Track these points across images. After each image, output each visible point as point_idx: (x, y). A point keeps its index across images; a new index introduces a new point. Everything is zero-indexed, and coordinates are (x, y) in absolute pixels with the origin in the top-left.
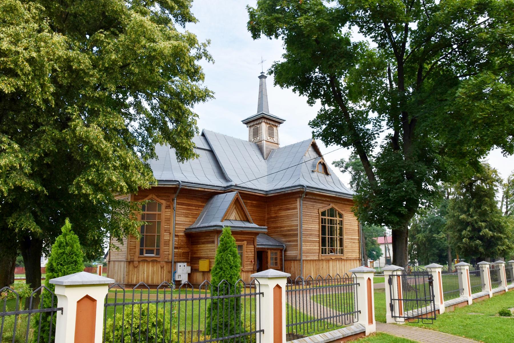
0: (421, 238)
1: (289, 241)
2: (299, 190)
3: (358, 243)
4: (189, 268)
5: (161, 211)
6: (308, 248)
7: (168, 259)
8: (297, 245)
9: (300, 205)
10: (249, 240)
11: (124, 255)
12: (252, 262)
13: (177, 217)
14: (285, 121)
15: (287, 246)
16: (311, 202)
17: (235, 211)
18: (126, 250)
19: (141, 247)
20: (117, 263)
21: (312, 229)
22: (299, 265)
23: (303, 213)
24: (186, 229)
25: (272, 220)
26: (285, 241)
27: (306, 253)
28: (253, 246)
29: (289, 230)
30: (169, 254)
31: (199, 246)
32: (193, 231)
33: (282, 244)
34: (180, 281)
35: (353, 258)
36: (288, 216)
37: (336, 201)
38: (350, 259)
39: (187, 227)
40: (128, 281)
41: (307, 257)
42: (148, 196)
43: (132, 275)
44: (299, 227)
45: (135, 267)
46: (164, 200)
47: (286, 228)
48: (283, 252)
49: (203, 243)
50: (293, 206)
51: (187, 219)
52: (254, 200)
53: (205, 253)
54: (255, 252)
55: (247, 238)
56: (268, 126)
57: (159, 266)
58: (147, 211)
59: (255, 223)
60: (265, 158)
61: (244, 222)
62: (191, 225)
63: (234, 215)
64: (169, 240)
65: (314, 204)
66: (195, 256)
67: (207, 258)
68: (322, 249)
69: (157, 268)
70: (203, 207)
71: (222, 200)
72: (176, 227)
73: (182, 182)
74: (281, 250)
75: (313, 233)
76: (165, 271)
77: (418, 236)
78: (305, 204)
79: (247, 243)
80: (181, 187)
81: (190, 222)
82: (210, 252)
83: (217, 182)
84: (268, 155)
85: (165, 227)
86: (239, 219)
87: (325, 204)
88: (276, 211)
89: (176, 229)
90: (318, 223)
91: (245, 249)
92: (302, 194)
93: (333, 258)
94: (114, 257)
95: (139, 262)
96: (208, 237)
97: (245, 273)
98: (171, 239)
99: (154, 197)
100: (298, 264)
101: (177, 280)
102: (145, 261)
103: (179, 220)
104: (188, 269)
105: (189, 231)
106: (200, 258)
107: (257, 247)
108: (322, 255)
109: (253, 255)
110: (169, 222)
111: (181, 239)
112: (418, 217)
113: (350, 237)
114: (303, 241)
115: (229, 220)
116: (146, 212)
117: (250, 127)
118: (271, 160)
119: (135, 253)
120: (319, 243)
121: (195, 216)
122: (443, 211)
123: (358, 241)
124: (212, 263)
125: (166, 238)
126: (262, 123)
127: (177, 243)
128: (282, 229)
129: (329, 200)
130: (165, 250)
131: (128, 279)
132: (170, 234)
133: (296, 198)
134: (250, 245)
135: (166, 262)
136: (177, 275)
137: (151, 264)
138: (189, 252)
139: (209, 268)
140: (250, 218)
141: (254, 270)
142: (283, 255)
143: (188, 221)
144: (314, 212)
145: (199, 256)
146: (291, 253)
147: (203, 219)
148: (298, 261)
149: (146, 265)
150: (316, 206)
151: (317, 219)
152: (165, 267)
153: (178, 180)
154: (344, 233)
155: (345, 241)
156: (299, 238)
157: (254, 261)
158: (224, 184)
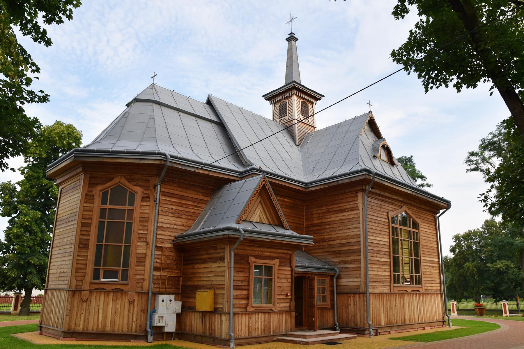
0: (471, 268)
1: (345, 262)
2: (363, 177)
3: (438, 269)
4: (180, 304)
6: (375, 273)
7: (142, 287)
8: (360, 267)
10: (283, 258)
12: (287, 295)
13: (160, 216)
14: (323, 96)
15: (342, 270)
16: (378, 200)
17: (260, 206)
18: (70, 270)
19: (95, 265)
20: (56, 293)
21: (380, 243)
22: (364, 301)
23: (368, 216)
24: (176, 237)
25: (315, 228)
26: (337, 262)
27: (373, 282)
28: (289, 269)
29: (344, 245)
30: (144, 280)
31: (196, 266)
32: (188, 240)
33: (333, 267)
34: (162, 327)
35: (433, 291)
36: (341, 222)
38: (430, 292)
39: (176, 234)
40: (69, 326)
41: (374, 289)
42: (113, 178)
43: (77, 314)
44: (362, 239)
45: (83, 301)
46: (140, 186)
47: (338, 242)
48: (335, 280)
49: (204, 261)
50: (351, 205)
51: (179, 221)
52: (288, 197)
53: (208, 279)
54: (292, 278)
55: (280, 255)
56: (300, 101)
57: (126, 300)
58: (110, 204)
59: (292, 229)
60: (297, 144)
61: (275, 227)
62: (186, 231)
63: (258, 214)
64: (146, 255)
65: (382, 203)
66: (189, 283)
67: (210, 288)
68: (394, 275)
69: (122, 304)
70: (206, 202)
71: (238, 190)
72: (159, 232)
73: (171, 156)
74: (332, 277)
76: (135, 310)
77: (466, 266)
78: (369, 203)
80: (168, 164)
81: (183, 225)
82: (216, 276)
83: (228, 164)
84: (301, 140)
85: (140, 232)
86: (267, 222)
87: (396, 205)
88: (321, 215)
89: (158, 237)
90: (387, 234)
91: (277, 272)
92: (366, 185)
93: (409, 290)
94: (54, 283)
95: (91, 292)
97: (276, 316)
98: (149, 253)
99: (123, 181)
100: (362, 300)
101: (156, 325)
102: (101, 290)
103: (163, 220)
104: (178, 306)
105: (180, 241)
106: (198, 287)
107: (296, 269)
108: (395, 285)
109: (289, 284)
110: (146, 224)
111: (167, 253)
112: (464, 242)
113: (429, 259)
114: (369, 262)
115: (250, 222)
116: (108, 206)
117: (275, 103)
118: (305, 146)
120: (390, 265)
121: (193, 217)
122: (514, 231)
123: (437, 265)
124: (219, 297)
125: (140, 252)
126: (293, 97)
127: (158, 261)
128: (332, 243)
129: (402, 200)
130: (138, 272)
131: (70, 321)
132: (148, 244)
133: (356, 192)
134: (284, 266)
135: (139, 293)
136: (156, 317)
137: (111, 295)
138: (180, 277)
139: (213, 306)
140: (284, 220)
141: (290, 309)
142: (335, 285)
143: (180, 223)
144: (382, 216)
145: (196, 283)
146: (347, 282)
147: (205, 221)
148: (361, 295)
150: (384, 207)
153: (165, 152)
154: (421, 252)
155: (422, 264)
156: (362, 257)
157: (291, 295)
158: (241, 169)
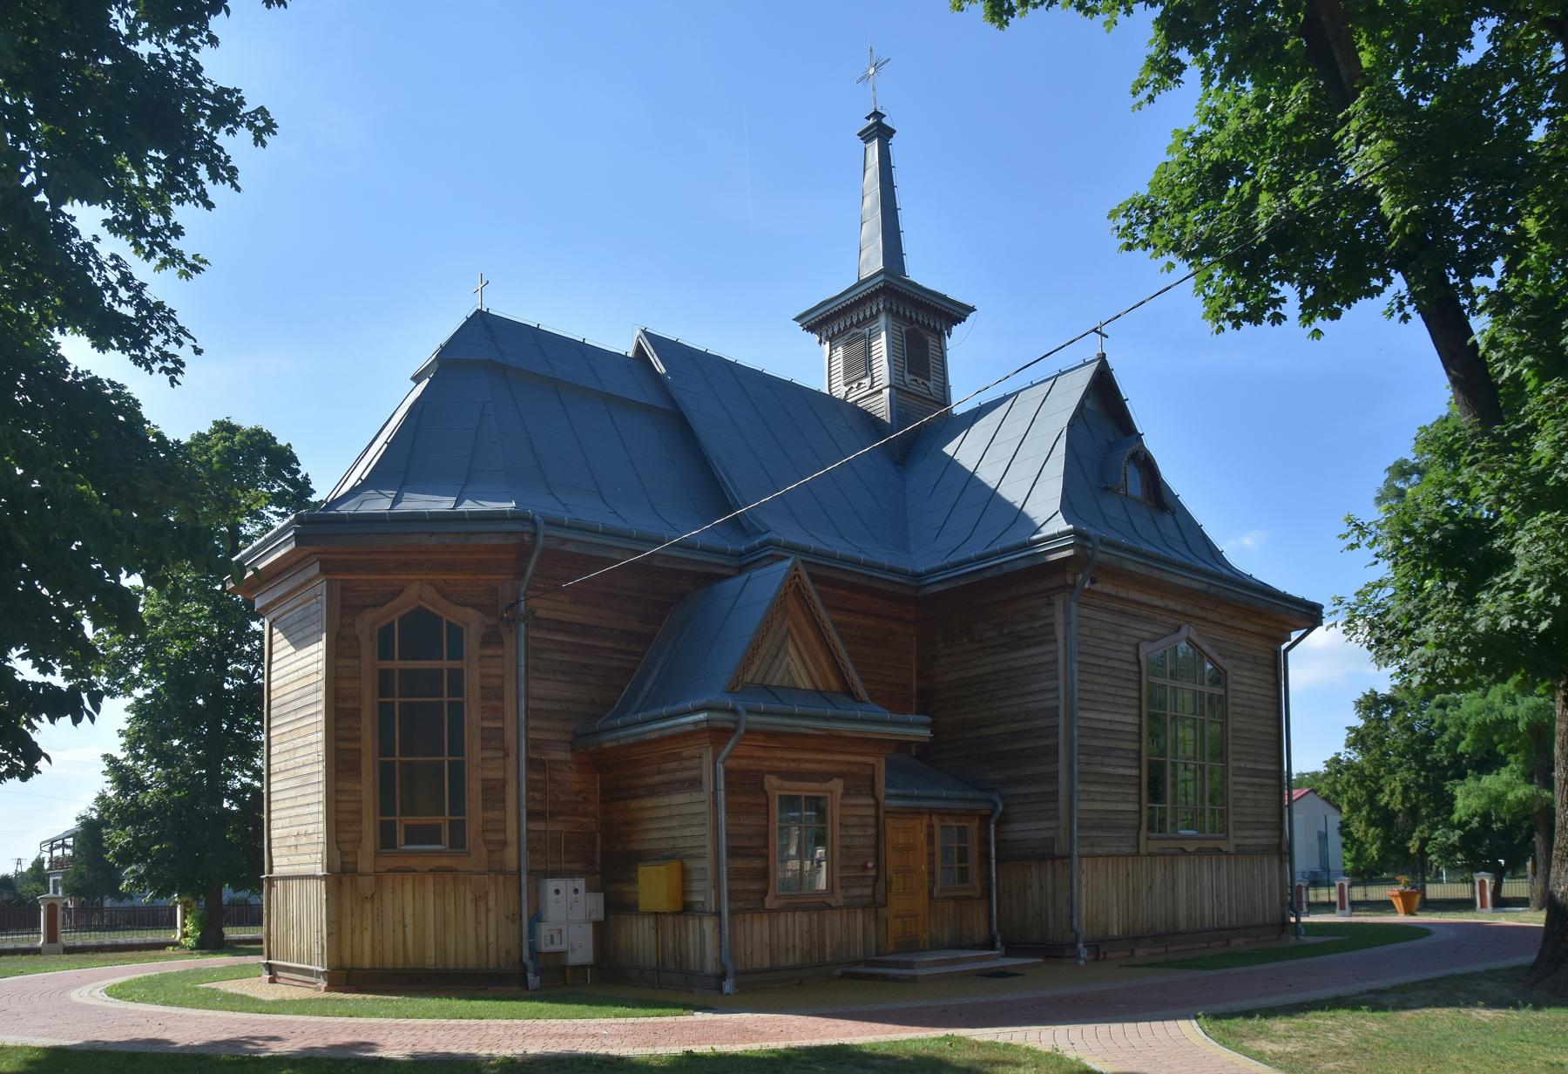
5: (461, 658)
6: (1097, 806)
8: (1056, 793)
9: (1068, 624)
11: (314, 848)
20: (295, 884)
28: (872, 802)
31: (633, 804)
37: (1203, 614)
49: (654, 791)
53: (663, 834)
64: (504, 782)
75: (1114, 744)
76: (492, 915)
79: (846, 789)
90: (1135, 702)
93: (1191, 847)
96: (672, 765)
101: (544, 949)
106: (325, 878)
108: (1151, 834)
113: (1251, 765)
119: (360, 840)
120: (1140, 785)
129: (1179, 608)
149: (408, 887)
151: (1131, 685)
152: (492, 897)
